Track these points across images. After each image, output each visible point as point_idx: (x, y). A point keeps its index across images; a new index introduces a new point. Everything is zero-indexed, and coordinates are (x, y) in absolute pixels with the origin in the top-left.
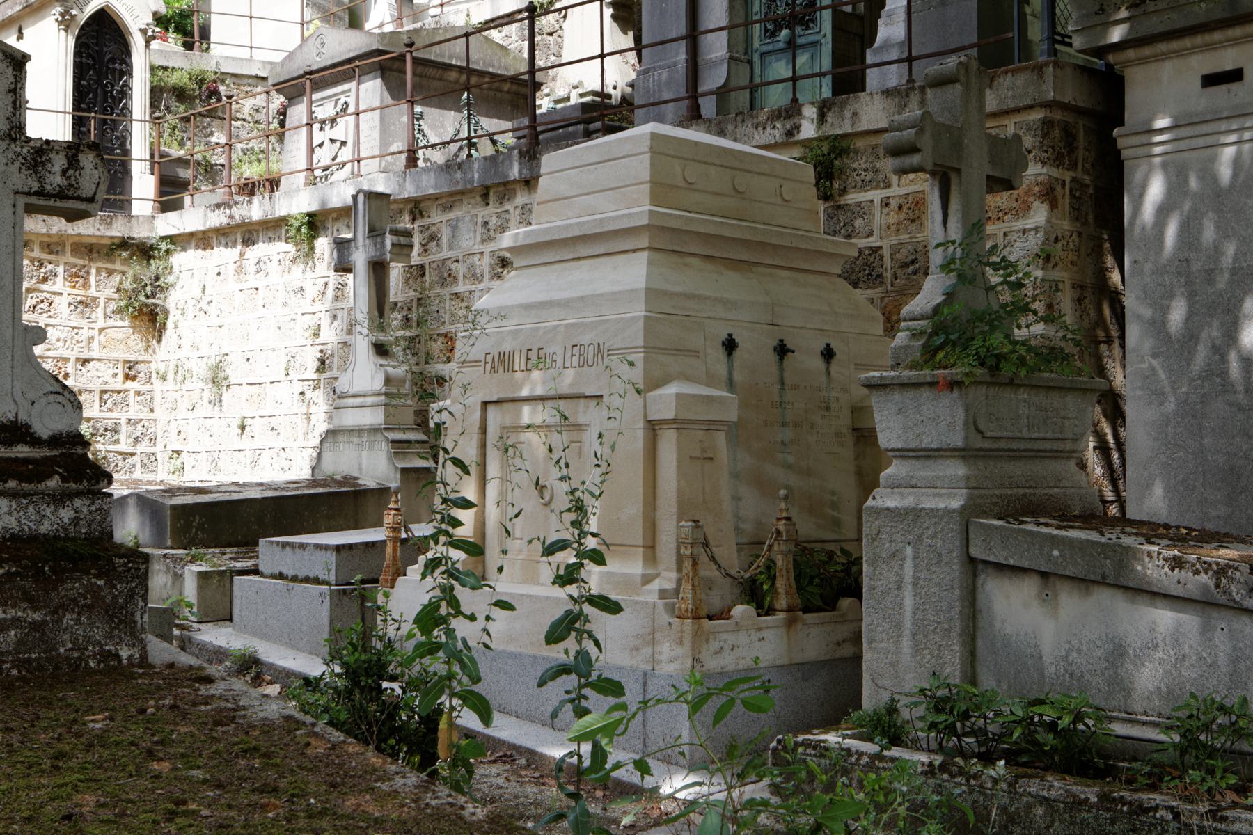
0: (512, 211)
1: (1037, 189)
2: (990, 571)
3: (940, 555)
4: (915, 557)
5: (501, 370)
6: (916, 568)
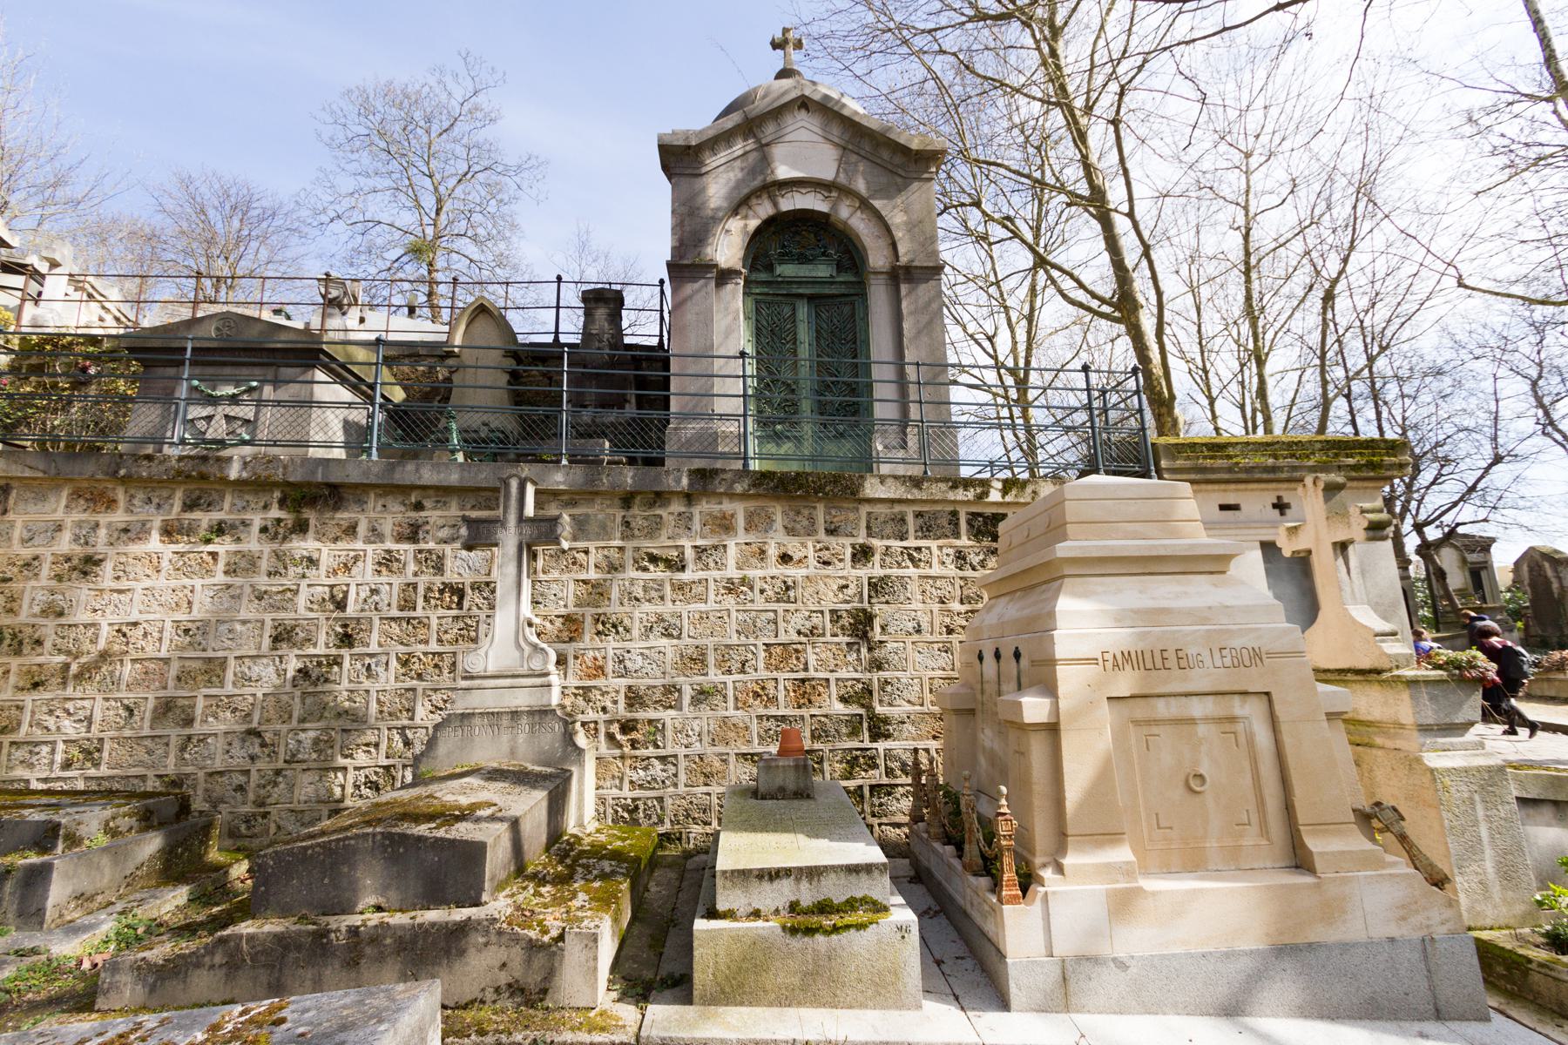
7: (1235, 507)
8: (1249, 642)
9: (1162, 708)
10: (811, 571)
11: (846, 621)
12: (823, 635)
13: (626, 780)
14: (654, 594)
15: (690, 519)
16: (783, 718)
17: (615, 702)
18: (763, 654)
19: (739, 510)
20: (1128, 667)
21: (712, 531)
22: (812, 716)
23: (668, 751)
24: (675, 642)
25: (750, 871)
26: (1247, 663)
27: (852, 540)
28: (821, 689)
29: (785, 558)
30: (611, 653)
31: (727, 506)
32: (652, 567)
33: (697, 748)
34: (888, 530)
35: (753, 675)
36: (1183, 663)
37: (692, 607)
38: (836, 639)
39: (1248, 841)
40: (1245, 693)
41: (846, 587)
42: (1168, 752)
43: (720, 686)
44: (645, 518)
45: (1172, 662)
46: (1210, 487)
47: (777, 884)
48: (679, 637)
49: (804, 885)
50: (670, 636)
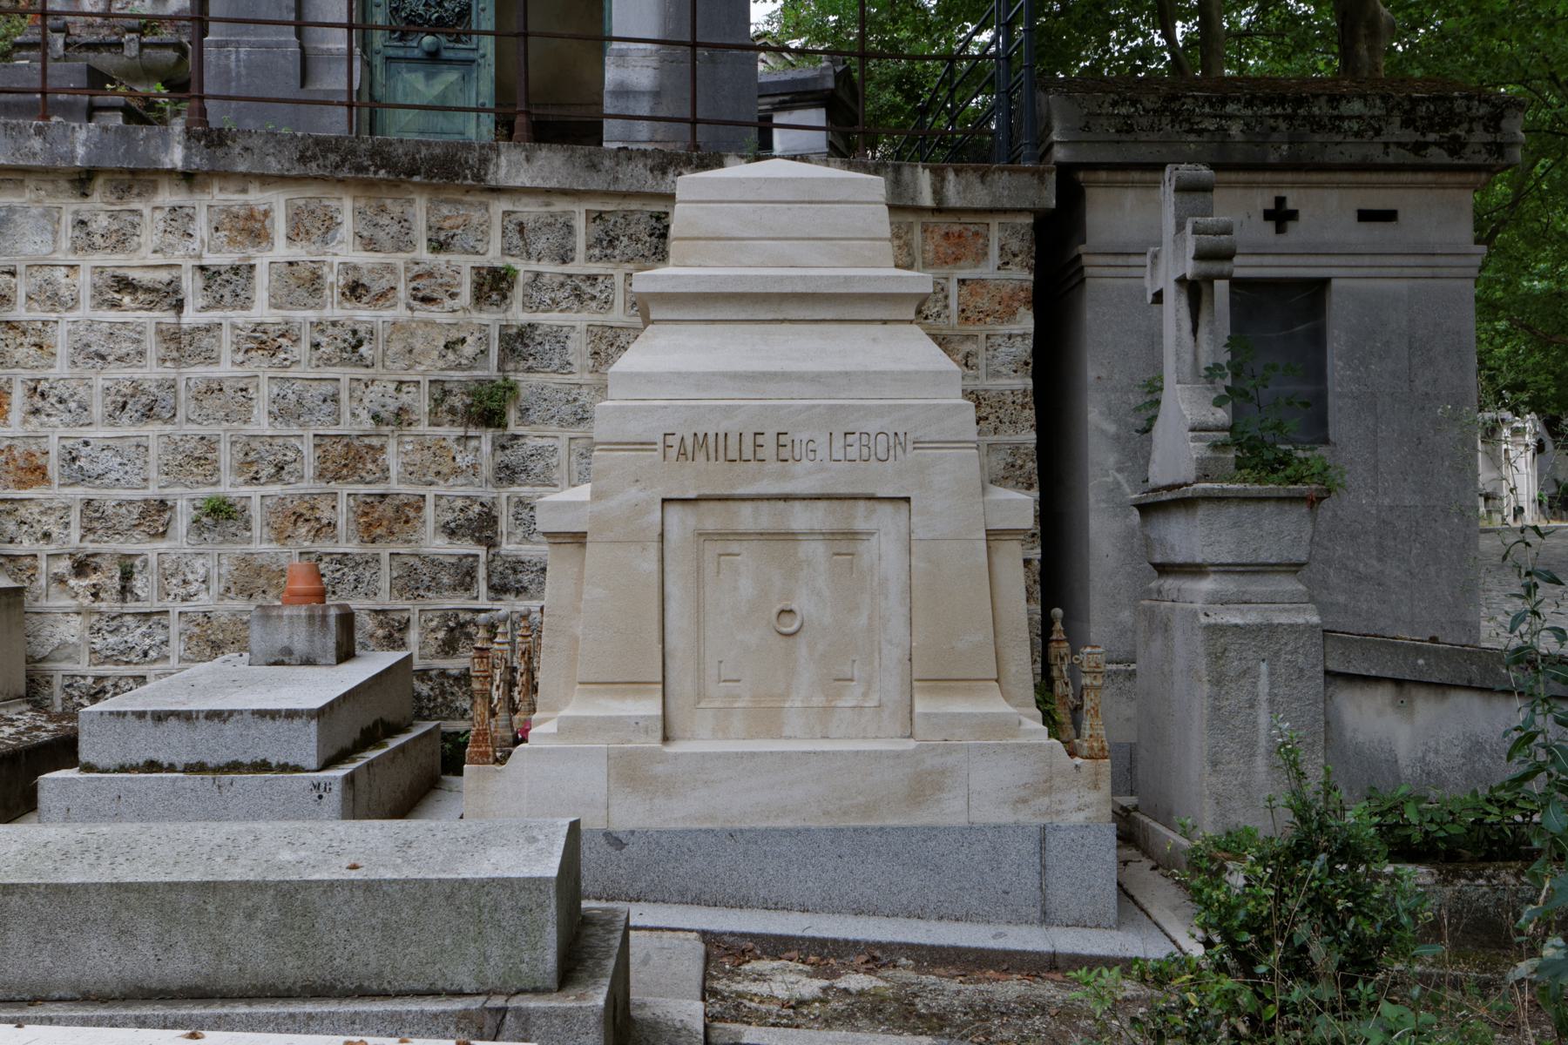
0: (146, 211)
1: (1022, 295)
2: (1339, 682)
3: (1301, 670)
4: (1271, 674)
5: (701, 457)
6: (1272, 685)
7: (1389, 216)
9: (746, 518)
10: (400, 313)
19: (276, 203)
20: (701, 457)
21: (232, 241)
29: (355, 290)
31: (256, 197)
36: (785, 453)
45: (769, 451)
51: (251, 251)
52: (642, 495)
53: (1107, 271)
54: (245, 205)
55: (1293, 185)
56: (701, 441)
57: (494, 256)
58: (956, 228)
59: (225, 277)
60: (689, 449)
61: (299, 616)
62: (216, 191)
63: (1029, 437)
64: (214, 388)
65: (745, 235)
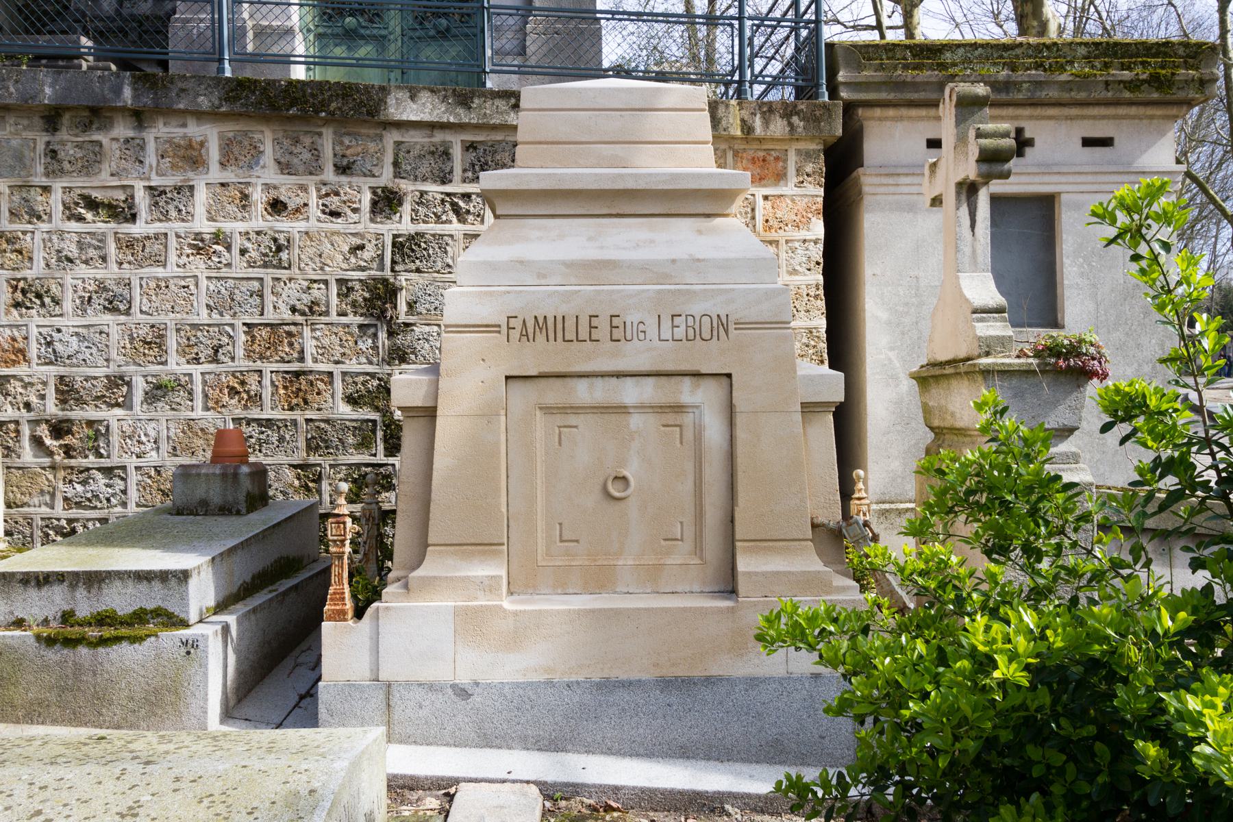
7: (1106, 142)
8: (715, 307)
9: (583, 392)
11: (360, 295)
12: (327, 313)
13: (59, 497)
14: (92, 253)
15: (142, 148)
16: (269, 423)
17: (43, 397)
18: (243, 338)
19: (211, 136)
20: (541, 338)
22: (308, 421)
23: (114, 461)
24: (123, 318)
25: (13, 574)
26: (706, 335)
27: (373, 182)
28: (321, 386)
29: (277, 206)
30: (34, 331)
31: (195, 130)
32: (89, 216)
33: (153, 458)
34: (424, 169)
35: (230, 366)
36: (617, 334)
37: (147, 271)
38: (344, 320)
39: (675, 559)
40: (697, 375)
41: (362, 247)
42: (586, 446)
43: (184, 379)
44: (79, 146)
45: (603, 332)
46: (914, 112)
47: (45, 591)
48: (127, 312)
49: (81, 593)
50: (115, 310)
51: (190, 174)
52: (60, 413)
53: (882, 190)
54: (184, 137)
55: (1031, 117)
56: (541, 324)
57: (386, 177)
58: (761, 154)
59: (169, 195)
60: (530, 331)
61: (214, 474)
62: (161, 125)
63: (822, 323)
64: (162, 286)
65: (583, 140)
